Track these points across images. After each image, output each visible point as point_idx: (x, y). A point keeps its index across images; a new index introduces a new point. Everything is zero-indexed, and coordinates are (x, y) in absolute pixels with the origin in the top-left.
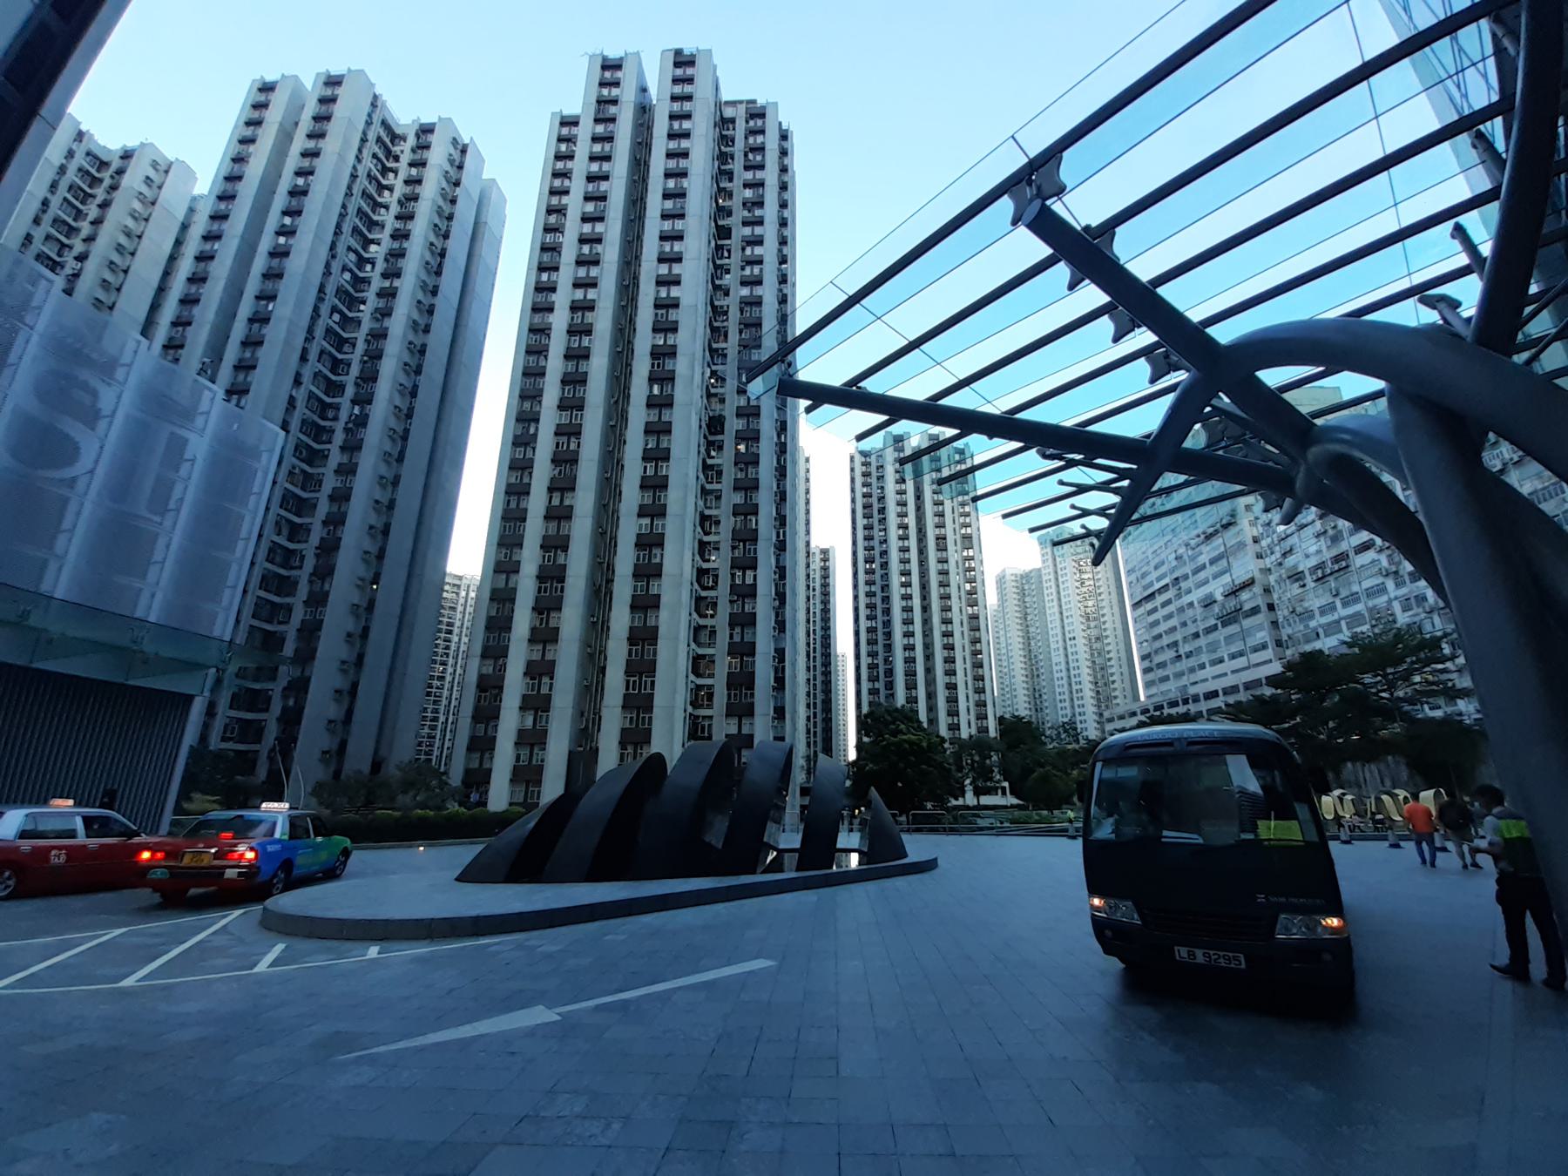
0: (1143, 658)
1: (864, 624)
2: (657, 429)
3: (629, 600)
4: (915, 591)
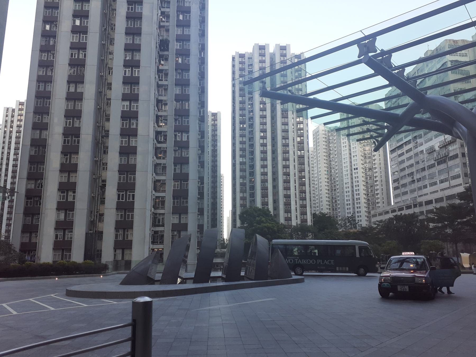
0: (394, 181)
1: (238, 159)
2: (132, 49)
3: (118, 149)
4: (269, 141)
